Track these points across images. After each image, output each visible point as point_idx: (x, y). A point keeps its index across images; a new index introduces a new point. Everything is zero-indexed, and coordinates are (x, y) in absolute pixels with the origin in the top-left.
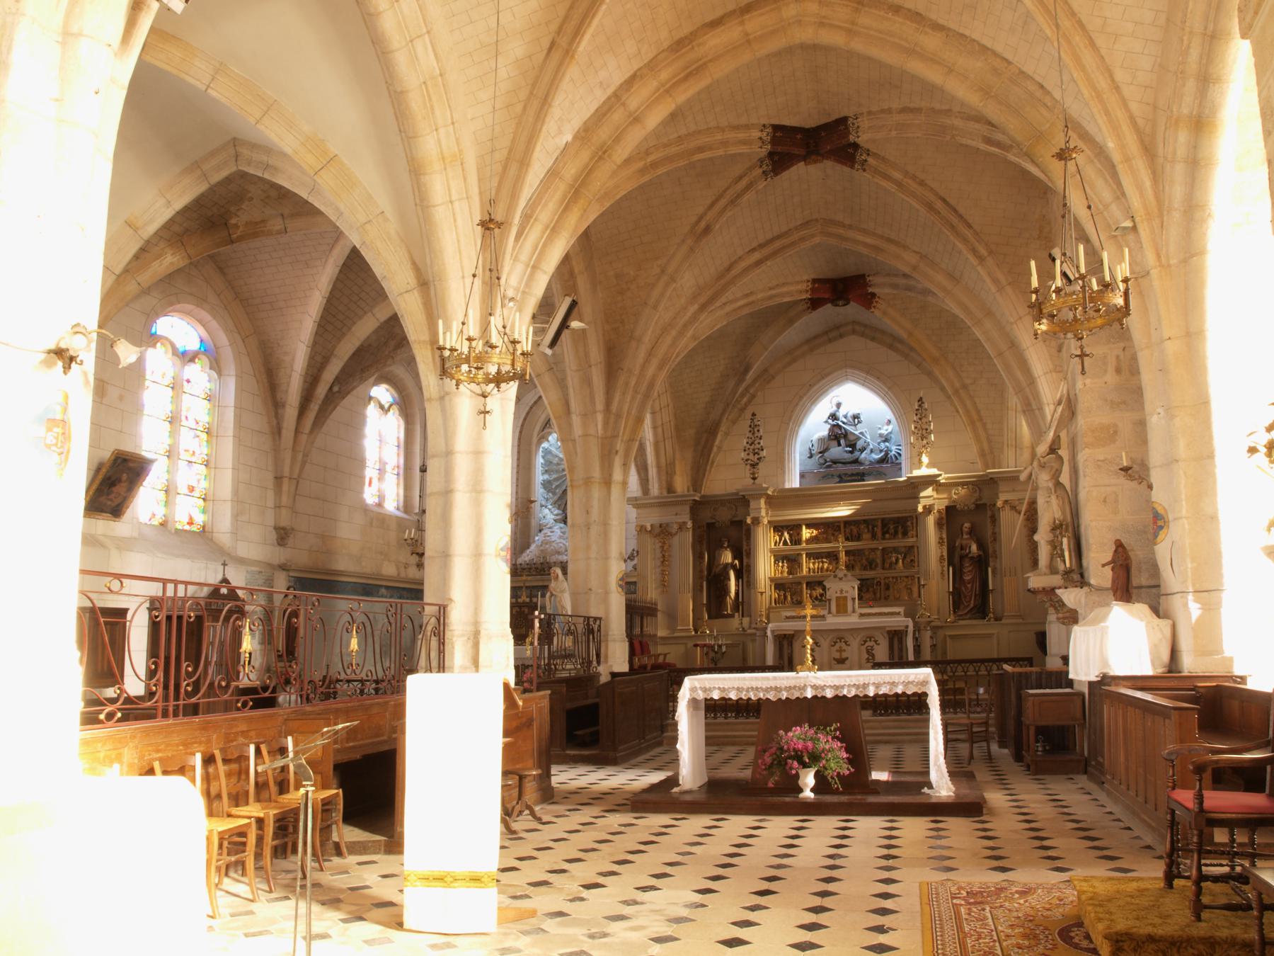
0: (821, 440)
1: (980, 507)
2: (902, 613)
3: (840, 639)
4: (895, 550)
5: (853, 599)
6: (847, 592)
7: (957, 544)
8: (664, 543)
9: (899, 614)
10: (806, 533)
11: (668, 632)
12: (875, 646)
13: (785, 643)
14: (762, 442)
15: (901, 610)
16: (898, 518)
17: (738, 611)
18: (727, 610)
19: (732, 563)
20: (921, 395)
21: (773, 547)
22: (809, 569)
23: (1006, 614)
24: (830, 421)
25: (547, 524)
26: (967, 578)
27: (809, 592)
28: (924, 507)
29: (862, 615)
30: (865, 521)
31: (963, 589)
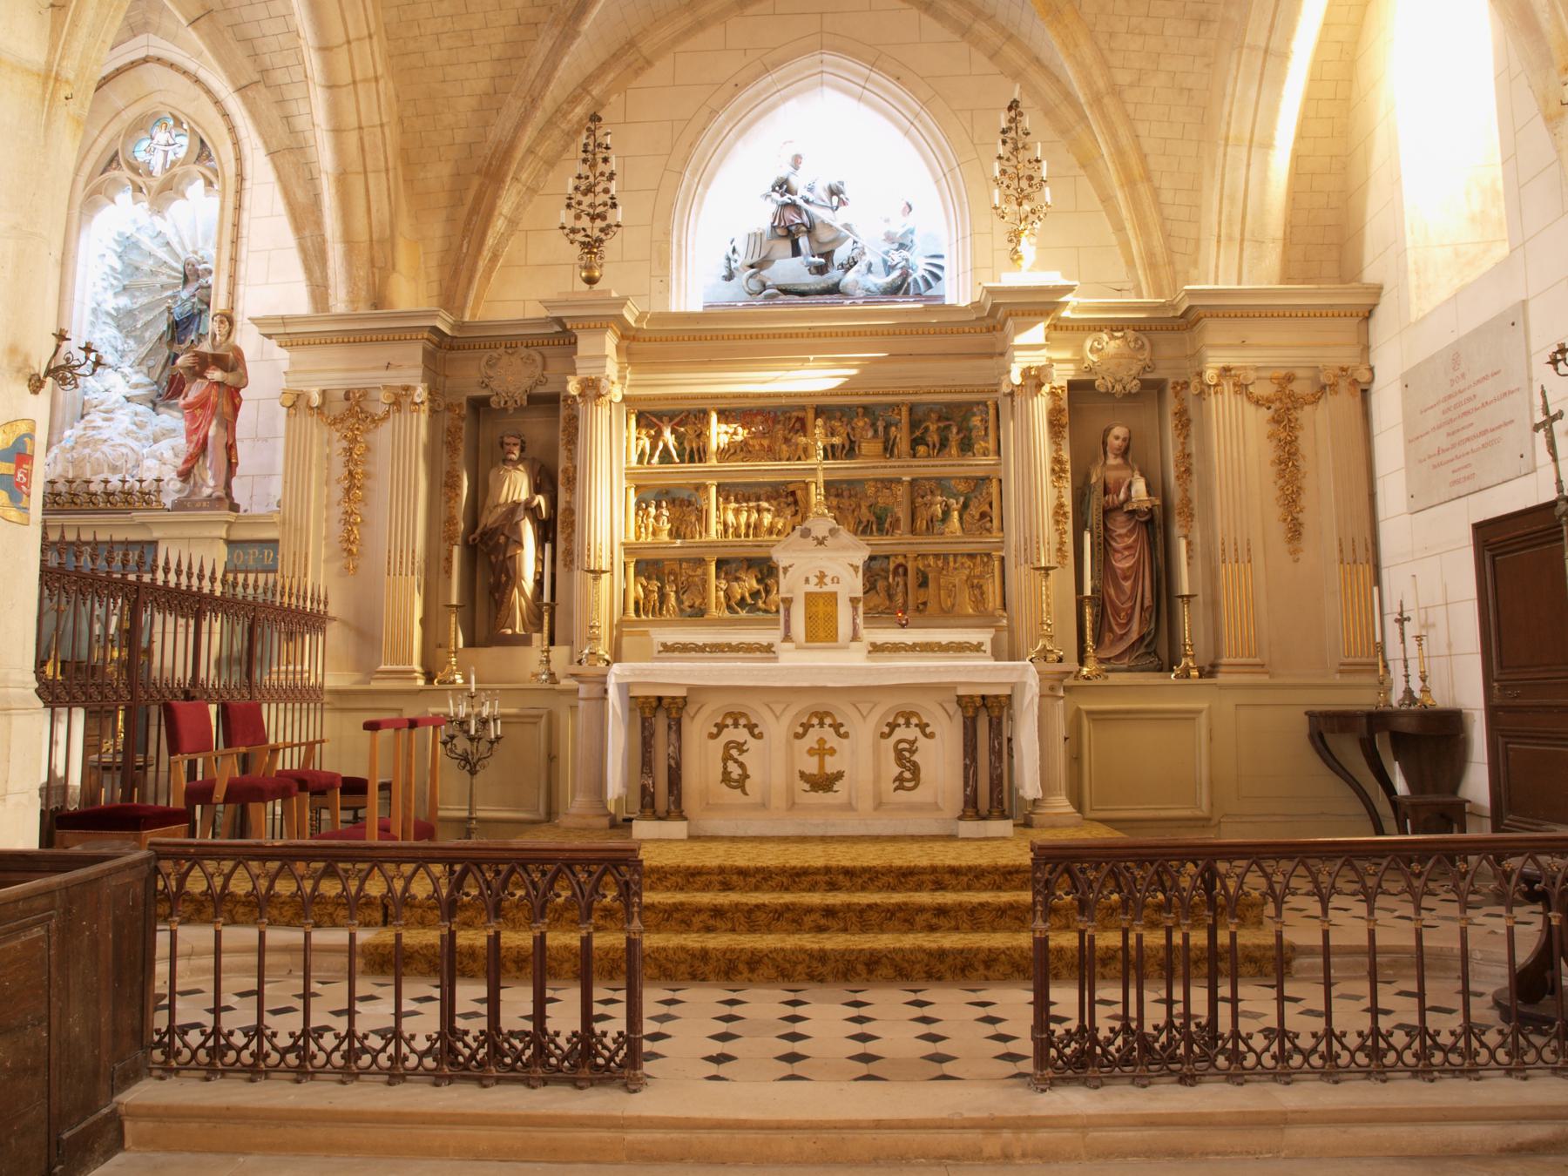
0: (756, 237)
1: (1152, 390)
2: (987, 647)
3: (821, 716)
4: (940, 484)
5: (854, 601)
6: (835, 580)
7: (1094, 480)
8: (354, 440)
9: (978, 648)
10: (719, 434)
11: (357, 676)
12: (922, 742)
13: (661, 723)
14: (613, 187)
15: (984, 636)
16: (948, 405)
17: (540, 630)
18: (513, 627)
19: (528, 502)
20: (1016, 96)
21: (634, 463)
22: (725, 524)
23: (1225, 660)
24: (776, 196)
25: (102, 403)
26: (1122, 563)
27: (723, 585)
28: (1026, 373)
29: (876, 648)
30: (867, 410)
31: (1112, 592)
